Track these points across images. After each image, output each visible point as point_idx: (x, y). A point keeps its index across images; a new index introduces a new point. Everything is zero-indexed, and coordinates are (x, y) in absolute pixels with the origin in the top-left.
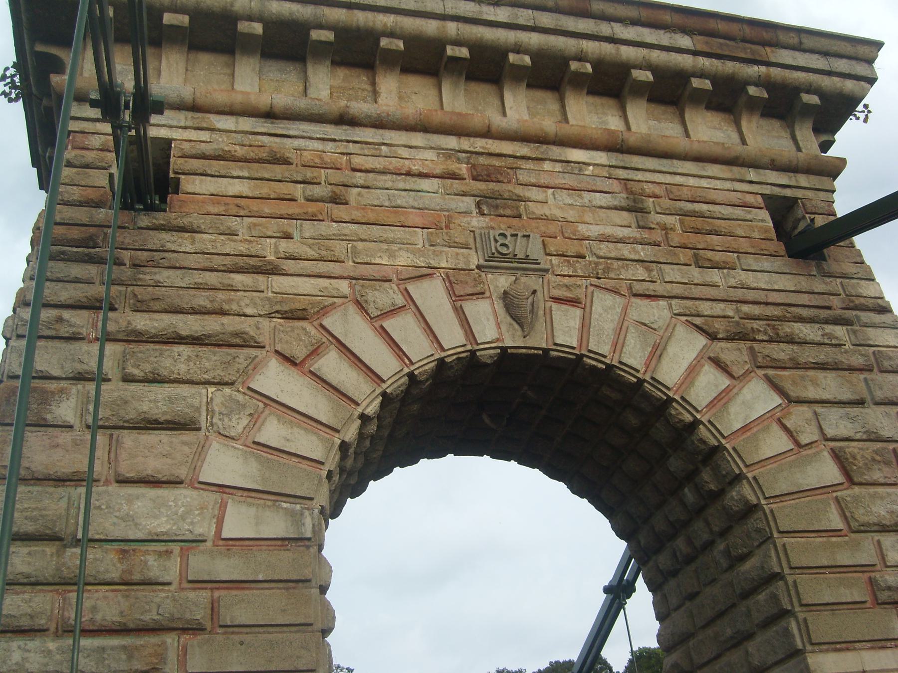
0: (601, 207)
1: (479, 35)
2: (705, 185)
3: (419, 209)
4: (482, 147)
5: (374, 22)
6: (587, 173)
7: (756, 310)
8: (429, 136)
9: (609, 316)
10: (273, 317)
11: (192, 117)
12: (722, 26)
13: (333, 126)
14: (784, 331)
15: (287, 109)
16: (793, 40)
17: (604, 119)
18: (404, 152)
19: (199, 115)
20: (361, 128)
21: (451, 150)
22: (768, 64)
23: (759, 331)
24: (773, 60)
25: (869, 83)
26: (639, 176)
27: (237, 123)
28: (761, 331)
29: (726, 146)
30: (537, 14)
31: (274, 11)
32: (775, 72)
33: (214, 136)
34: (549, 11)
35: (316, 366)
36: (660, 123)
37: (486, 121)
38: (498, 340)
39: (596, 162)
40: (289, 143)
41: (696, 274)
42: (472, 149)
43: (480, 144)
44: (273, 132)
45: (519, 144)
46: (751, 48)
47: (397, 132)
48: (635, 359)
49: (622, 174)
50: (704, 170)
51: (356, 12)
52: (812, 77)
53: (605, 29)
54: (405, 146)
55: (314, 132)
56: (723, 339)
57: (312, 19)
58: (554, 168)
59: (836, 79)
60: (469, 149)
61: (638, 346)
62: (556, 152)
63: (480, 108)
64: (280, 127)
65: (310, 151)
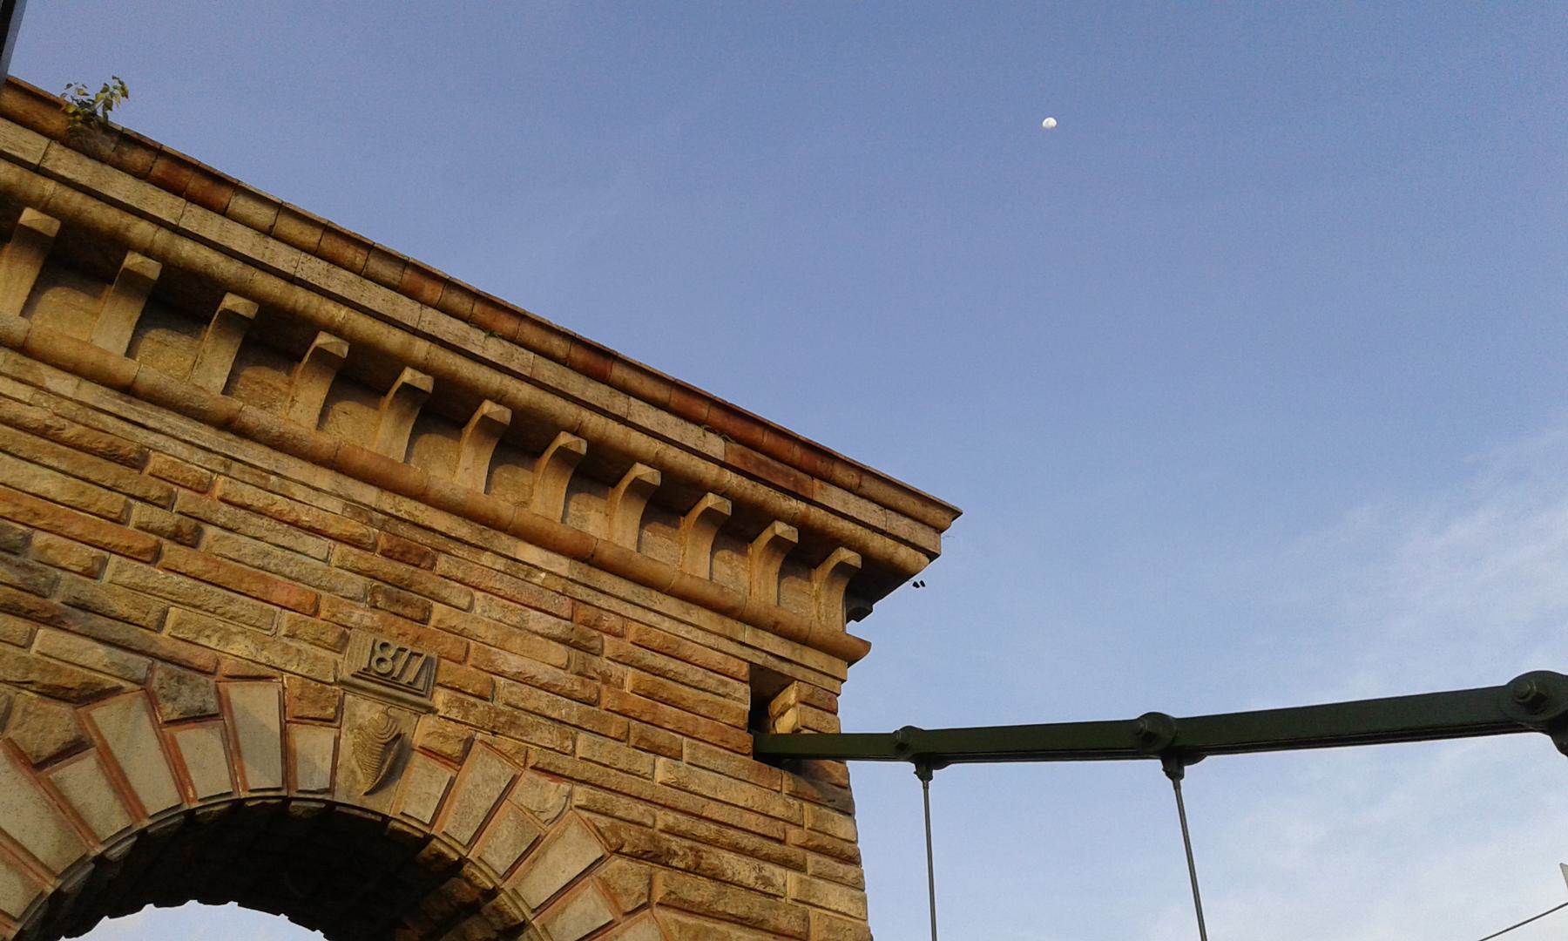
0: (536, 633)
1: (454, 368)
2: (683, 634)
3: (290, 578)
4: (409, 513)
5: (318, 309)
6: (535, 580)
7: (685, 823)
8: (341, 478)
9: (488, 790)
10: (24, 688)
11: (15, 361)
12: (767, 440)
13: (213, 430)
14: (708, 861)
15: (156, 391)
16: (850, 478)
17: (583, 513)
18: (299, 493)
19: (28, 361)
20: (251, 443)
21: (365, 505)
22: (811, 502)
23: (676, 854)
24: (818, 499)
25: (928, 556)
26: (603, 602)
27: (78, 387)
28: (678, 855)
29: (726, 590)
30: (540, 360)
31: (184, 255)
32: (817, 515)
33: (38, 396)
34: (556, 362)
35: (60, 773)
36: (654, 536)
37: (425, 481)
38: (326, 791)
39: (552, 570)
40: (141, 436)
41: (624, 755)
42: (393, 511)
43: (407, 507)
44: (124, 414)
45: (460, 520)
46: (796, 476)
47: (300, 461)
48: (501, 857)
49: (581, 592)
50: (688, 613)
51: (298, 289)
52: (860, 532)
53: (620, 404)
54: (304, 484)
55: (185, 431)
56: (626, 854)
57: (233, 280)
58: (494, 563)
59: (889, 542)
60: (389, 511)
61: (511, 841)
62: (505, 542)
63: (426, 456)
64: (137, 411)
65: (169, 455)
